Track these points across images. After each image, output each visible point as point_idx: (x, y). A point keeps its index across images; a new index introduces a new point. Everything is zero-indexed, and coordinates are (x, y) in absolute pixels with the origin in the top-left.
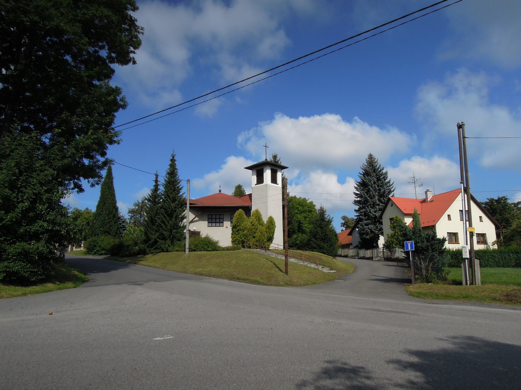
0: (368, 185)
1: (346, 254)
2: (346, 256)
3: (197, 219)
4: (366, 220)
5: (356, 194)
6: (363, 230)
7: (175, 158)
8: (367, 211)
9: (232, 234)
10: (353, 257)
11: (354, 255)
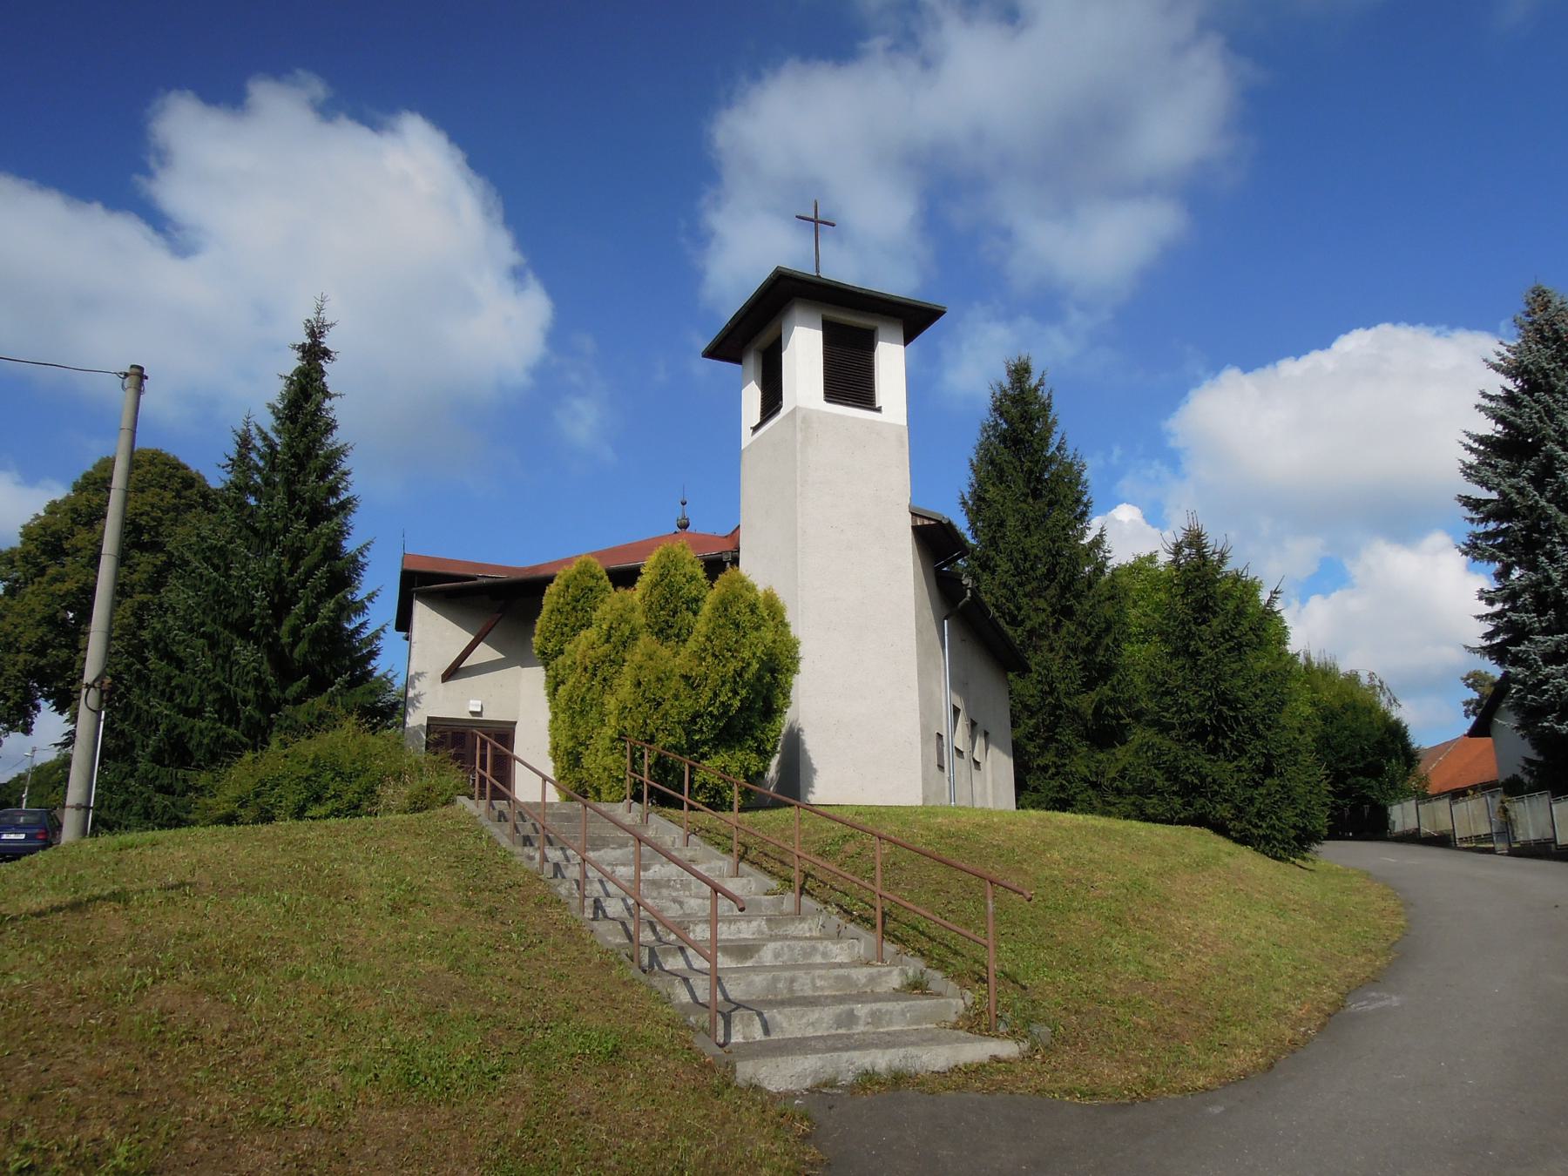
0: (1541, 442)
1: (1444, 825)
2: (1443, 841)
3: (485, 653)
4: (1546, 631)
5: (1468, 502)
6: (1537, 688)
7: (328, 342)
8: (1549, 581)
9: (552, 722)
10: (1480, 846)
11: (1484, 829)
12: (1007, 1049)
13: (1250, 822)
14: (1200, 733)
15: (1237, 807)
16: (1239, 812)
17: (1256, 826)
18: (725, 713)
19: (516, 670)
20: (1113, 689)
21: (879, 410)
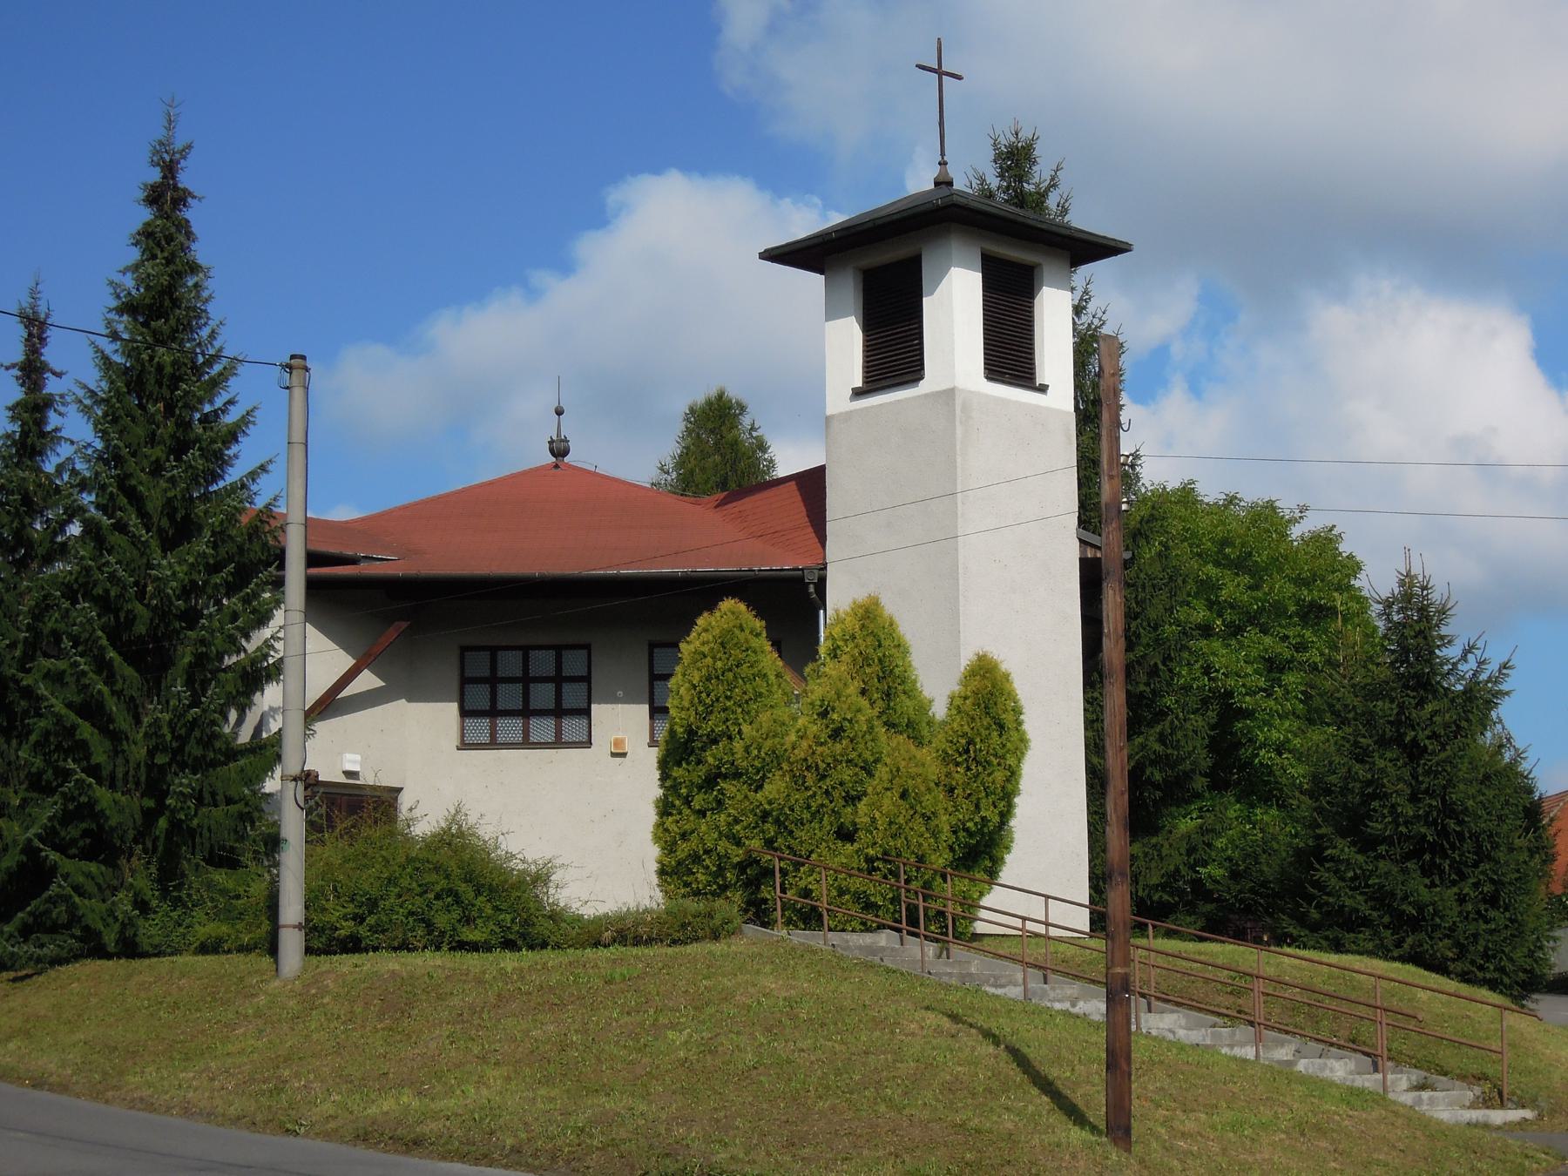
3: (367, 681)
7: (185, 180)
12: (1528, 1114)
13: (1473, 962)
14: (1418, 849)
15: (1458, 944)
16: (1462, 951)
17: (1481, 968)
18: (980, 831)
19: (401, 709)
20: (1162, 739)
21: (1043, 389)
